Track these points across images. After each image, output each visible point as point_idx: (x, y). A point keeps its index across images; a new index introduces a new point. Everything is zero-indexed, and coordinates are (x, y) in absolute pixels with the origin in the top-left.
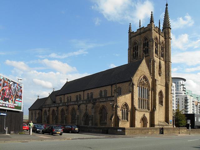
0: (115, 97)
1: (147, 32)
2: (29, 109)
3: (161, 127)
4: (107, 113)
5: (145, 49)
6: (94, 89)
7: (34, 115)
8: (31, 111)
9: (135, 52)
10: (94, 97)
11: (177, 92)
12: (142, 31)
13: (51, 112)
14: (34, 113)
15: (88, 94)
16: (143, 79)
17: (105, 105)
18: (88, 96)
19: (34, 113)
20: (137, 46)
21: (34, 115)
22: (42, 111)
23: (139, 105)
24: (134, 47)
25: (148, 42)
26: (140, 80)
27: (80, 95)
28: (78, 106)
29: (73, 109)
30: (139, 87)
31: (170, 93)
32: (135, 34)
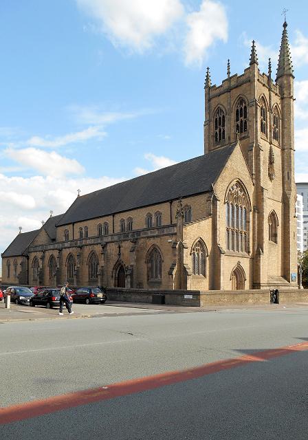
1: (244, 85)
2: (2, 255)
4: (161, 261)
5: (239, 123)
7: (12, 267)
8: (6, 260)
10: (135, 228)
12: (233, 83)
13: (64, 259)
14: (12, 263)
15: (123, 221)
19: (12, 263)
20: (224, 117)
21: (12, 267)
26: (230, 190)
29: (93, 253)
30: (228, 204)
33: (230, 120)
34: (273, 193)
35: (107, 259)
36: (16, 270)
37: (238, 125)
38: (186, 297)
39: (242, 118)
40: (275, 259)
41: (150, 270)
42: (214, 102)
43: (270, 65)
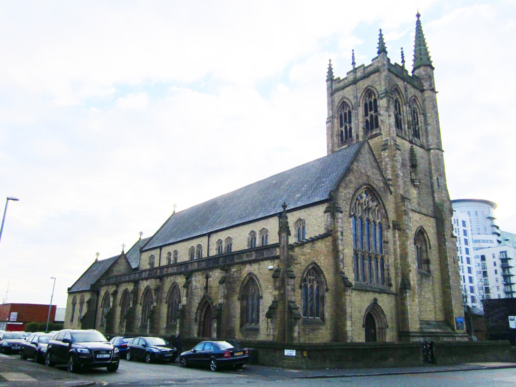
0: (282, 246)
1: (372, 76)
2: (69, 289)
3: (428, 339)
4: (260, 297)
5: (368, 118)
6: (232, 230)
7: (78, 307)
8: (72, 296)
9: (344, 126)
10: (234, 249)
11: (478, 237)
12: (359, 74)
13: (119, 296)
14: (78, 301)
15: (220, 242)
16: (364, 195)
17: (256, 273)
18: (219, 249)
19: (78, 301)
20: (350, 112)
21: (78, 307)
22: (98, 293)
23: (358, 270)
24: (341, 115)
25: (375, 101)
26: (357, 199)
27: (199, 246)
28: (187, 279)
29: (175, 286)
30: (355, 217)
31: (449, 235)
32: (342, 84)
33: (357, 115)
34: (419, 204)
35: (190, 295)
36: (81, 310)
37: (367, 121)
38: (287, 352)
39: (372, 112)
40: (429, 295)
41: (244, 311)
42: (338, 97)
43: (402, 55)
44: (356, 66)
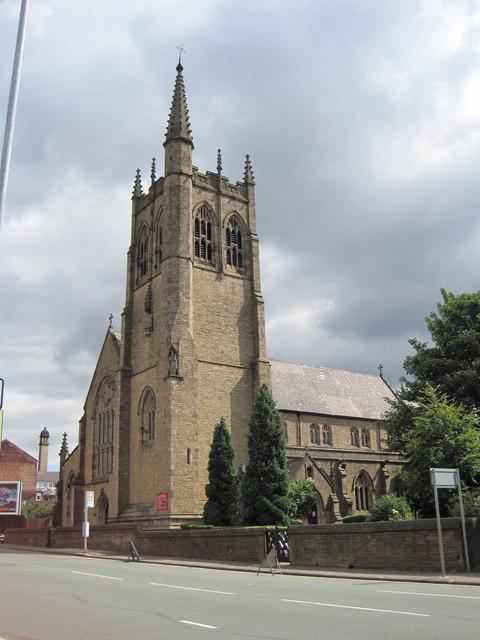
44: (156, 180)
